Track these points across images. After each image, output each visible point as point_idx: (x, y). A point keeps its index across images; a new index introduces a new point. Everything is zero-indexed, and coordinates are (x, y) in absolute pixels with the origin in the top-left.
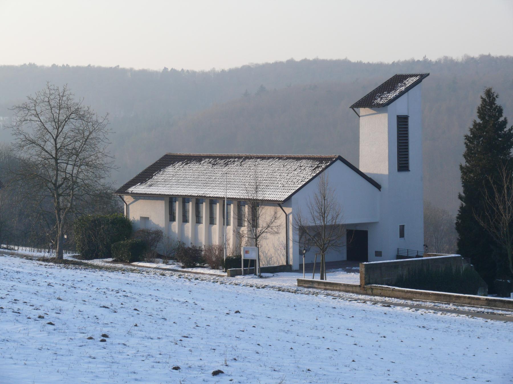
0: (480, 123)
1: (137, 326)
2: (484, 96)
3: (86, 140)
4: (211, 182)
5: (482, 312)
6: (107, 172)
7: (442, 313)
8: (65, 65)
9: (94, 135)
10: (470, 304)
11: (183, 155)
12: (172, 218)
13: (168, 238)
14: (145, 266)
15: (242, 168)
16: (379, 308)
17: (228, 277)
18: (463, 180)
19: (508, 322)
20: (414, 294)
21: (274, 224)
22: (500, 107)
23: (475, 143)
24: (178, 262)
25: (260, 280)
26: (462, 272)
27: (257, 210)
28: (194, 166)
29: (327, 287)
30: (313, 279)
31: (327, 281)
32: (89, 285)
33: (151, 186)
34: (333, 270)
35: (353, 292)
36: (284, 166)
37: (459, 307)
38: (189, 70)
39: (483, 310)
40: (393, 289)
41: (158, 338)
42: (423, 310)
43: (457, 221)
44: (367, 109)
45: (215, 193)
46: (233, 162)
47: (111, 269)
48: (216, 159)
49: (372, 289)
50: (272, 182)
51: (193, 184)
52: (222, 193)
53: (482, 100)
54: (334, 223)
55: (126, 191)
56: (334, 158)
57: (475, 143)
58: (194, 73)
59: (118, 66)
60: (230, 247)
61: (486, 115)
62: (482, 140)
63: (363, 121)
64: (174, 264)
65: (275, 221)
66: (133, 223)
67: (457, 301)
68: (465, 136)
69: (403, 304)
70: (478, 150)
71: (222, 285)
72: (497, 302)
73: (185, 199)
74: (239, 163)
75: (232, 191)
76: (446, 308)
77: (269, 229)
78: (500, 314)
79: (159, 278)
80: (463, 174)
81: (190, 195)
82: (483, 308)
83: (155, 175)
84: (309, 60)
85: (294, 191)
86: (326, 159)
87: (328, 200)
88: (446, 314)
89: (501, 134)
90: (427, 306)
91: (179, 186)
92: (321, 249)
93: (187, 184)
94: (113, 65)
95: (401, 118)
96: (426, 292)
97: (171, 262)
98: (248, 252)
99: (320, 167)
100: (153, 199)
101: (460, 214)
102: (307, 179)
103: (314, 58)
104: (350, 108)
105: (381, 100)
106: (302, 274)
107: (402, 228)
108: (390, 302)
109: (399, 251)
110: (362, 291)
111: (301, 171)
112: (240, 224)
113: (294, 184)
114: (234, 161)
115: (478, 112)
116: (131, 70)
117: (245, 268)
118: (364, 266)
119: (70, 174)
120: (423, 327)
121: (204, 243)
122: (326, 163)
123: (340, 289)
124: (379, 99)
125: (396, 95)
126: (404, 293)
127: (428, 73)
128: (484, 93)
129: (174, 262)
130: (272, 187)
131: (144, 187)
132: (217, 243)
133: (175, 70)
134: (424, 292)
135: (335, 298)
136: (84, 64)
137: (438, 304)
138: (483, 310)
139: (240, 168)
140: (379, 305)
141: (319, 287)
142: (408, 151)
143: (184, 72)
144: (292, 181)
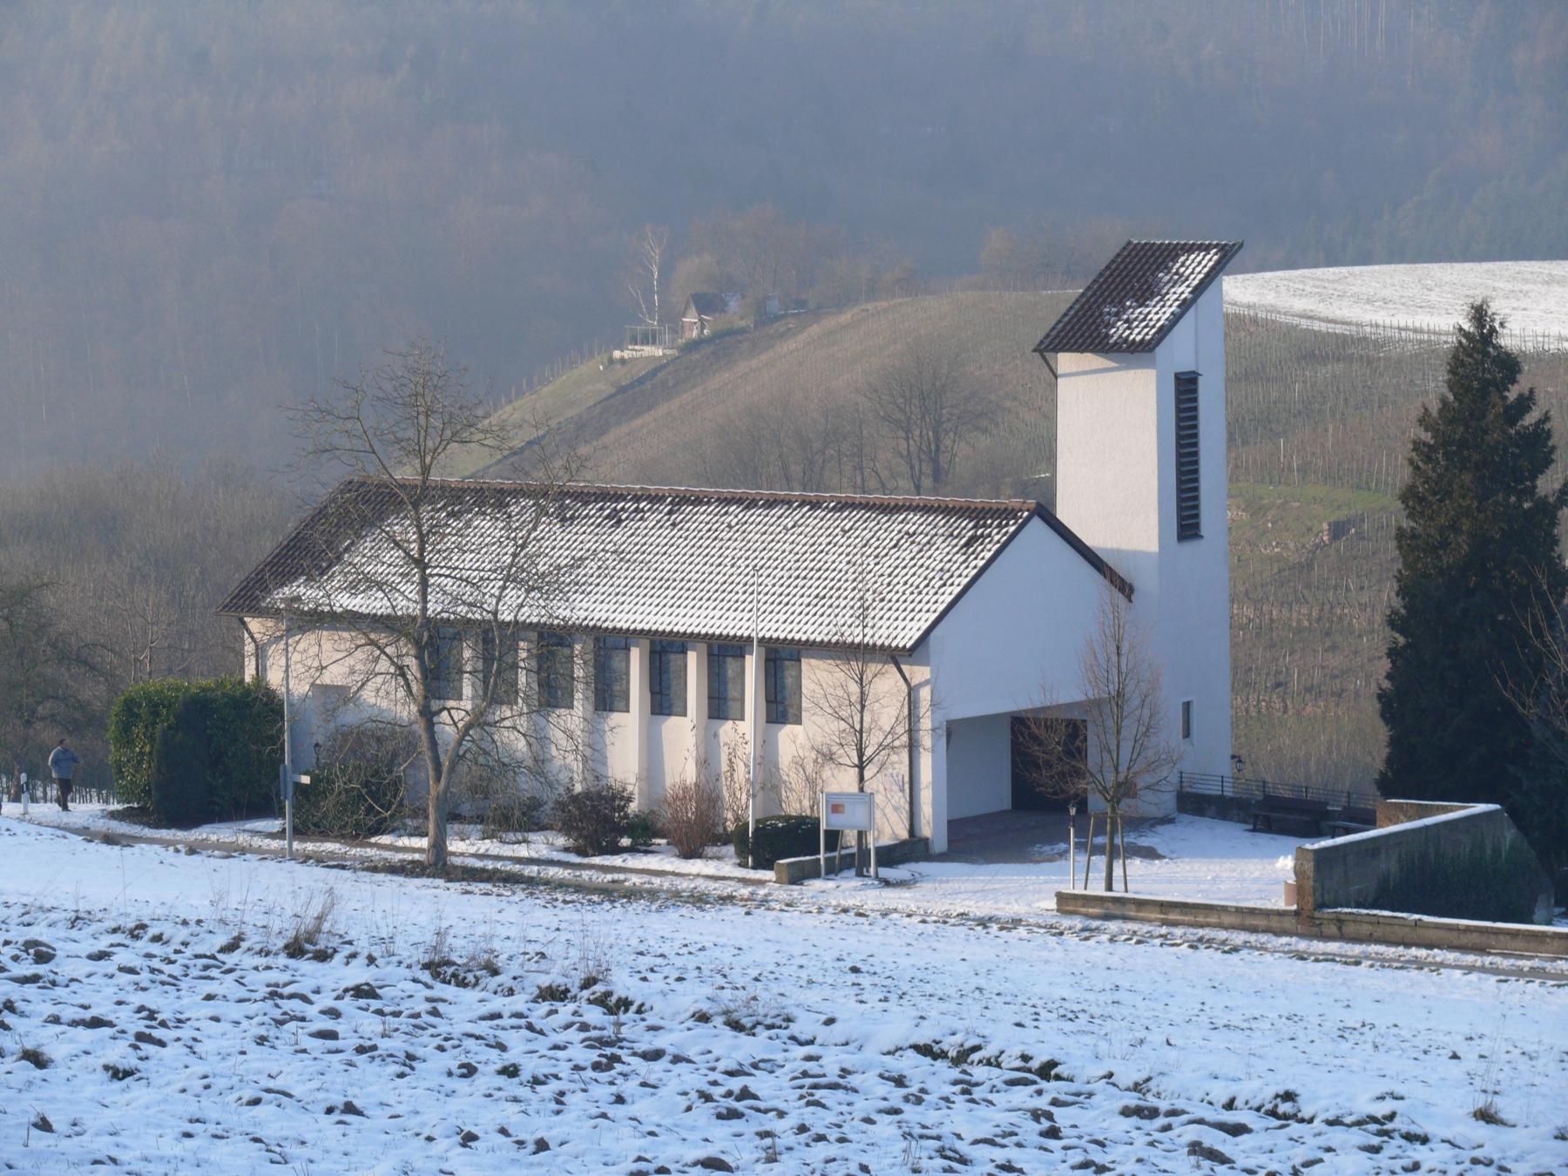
20: (1492, 936)
29: (1172, 917)
44: (1089, 356)
63: (1067, 391)
125: (1172, 313)
126: (1455, 934)
141: (1141, 915)
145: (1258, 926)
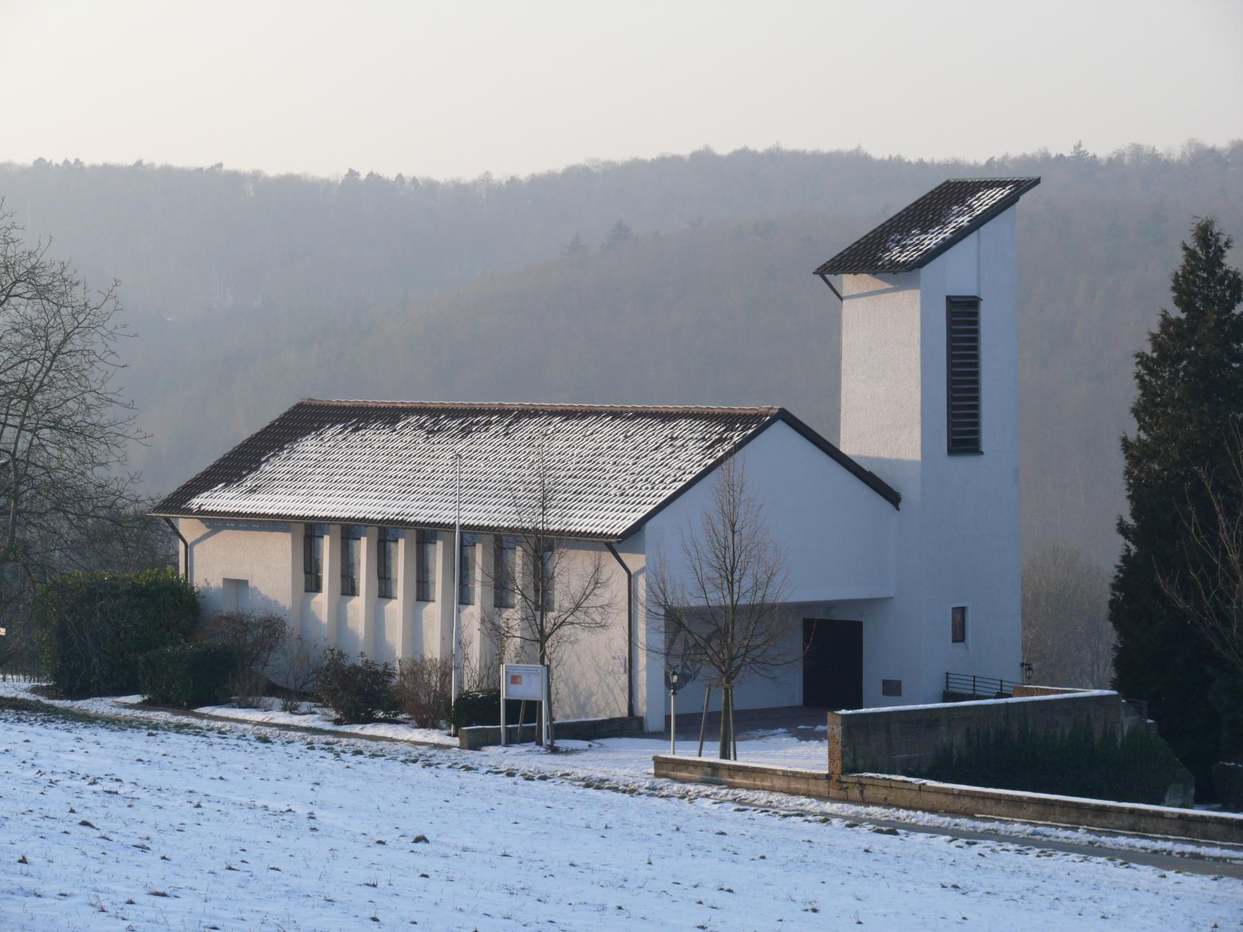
0: (1178, 319)
1: (26, 863)
2: (1192, 243)
3: (55, 356)
4: (422, 482)
5: (1165, 850)
6: (114, 449)
7: (1042, 852)
8: (72, 162)
9: (77, 342)
10: (1133, 830)
11: (347, 404)
12: (312, 584)
13: (300, 638)
14: (231, 717)
15: (508, 442)
16: (864, 836)
17: (463, 751)
18: (1131, 481)
19: (1226, 879)
20: (981, 802)
21: (592, 601)
22: (1235, 274)
23: (1166, 375)
24: (326, 706)
25: (551, 758)
26: (1120, 740)
27: (545, 561)
28: (376, 436)
29: (738, 780)
30: (700, 755)
31: (740, 762)
32: (24, 762)
33: (255, 491)
34: (761, 732)
35: (808, 795)
36: (626, 437)
37: (1103, 838)
38: (417, 177)
39: (1168, 845)
40: (920, 786)
41: (61, 895)
42: (989, 843)
43: (1114, 595)
45: (432, 512)
46: (485, 425)
47: (120, 721)
48: (439, 416)
49: (862, 786)
50: (590, 481)
51: (373, 486)
52: (451, 513)
53: (1184, 253)
54: (758, 600)
55: (184, 506)
56: (767, 416)
57: (1166, 375)
58: (431, 186)
59: (220, 165)
60: (473, 666)
61: (1196, 295)
62: (1185, 367)
63: (850, 310)
64: (314, 713)
65: (596, 591)
66: (203, 597)
67: (1098, 821)
68: (1137, 356)
69: (946, 828)
70: (1174, 396)
71: (427, 768)
72: (1210, 825)
73: (349, 529)
74: (500, 428)
75: (480, 507)
76: (1065, 840)
77: (578, 613)
78: (1217, 859)
79: (249, 749)
80: (1129, 464)
81: (362, 516)
82: (1168, 840)
83: (267, 460)
84: (754, 153)
85: (651, 507)
86: (745, 419)
87: (745, 532)
88: (1050, 855)
89: (1238, 349)
90: (1014, 834)
91: (331, 492)
92: (721, 671)
93: (354, 486)
94: (206, 163)
95: (956, 302)
96: (1012, 796)
97: (305, 705)
98: (519, 679)
99: (726, 439)
100: (260, 529)
101: (1121, 575)
102: (690, 473)
103: (768, 147)
104: (814, 273)
105: (901, 252)
106: (668, 742)
107: (960, 614)
108: (910, 824)
109: (950, 680)
110: (833, 793)
111: (673, 452)
112: (501, 602)
113: (653, 488)
114: (489, 423)
115: (1174, 289)
116: (256, 176)
117: (509, 726)
118: (839, 721)
119: (9, 452)
120: (955, 887)
121: (399, 654)
122: (743, 430)
123: (772, 787)
124: (897, 249)
125: (943, 239)
127: (1036, 176)
128: (1193, 233)
129: (315, 706)
130: (591, 497)
131: (234, 494)
132: (437, 655)
133: (379, 176)
134: (1007, 795)
135: (742, 807)
136: (124, 157)
137: (1044, 828)
138: (1168, 845)
139: (505, 441)
140: (865, 829)
142: (977, 399)
143: (404, 182)
144: (647, 480)
145: (799, 789)
